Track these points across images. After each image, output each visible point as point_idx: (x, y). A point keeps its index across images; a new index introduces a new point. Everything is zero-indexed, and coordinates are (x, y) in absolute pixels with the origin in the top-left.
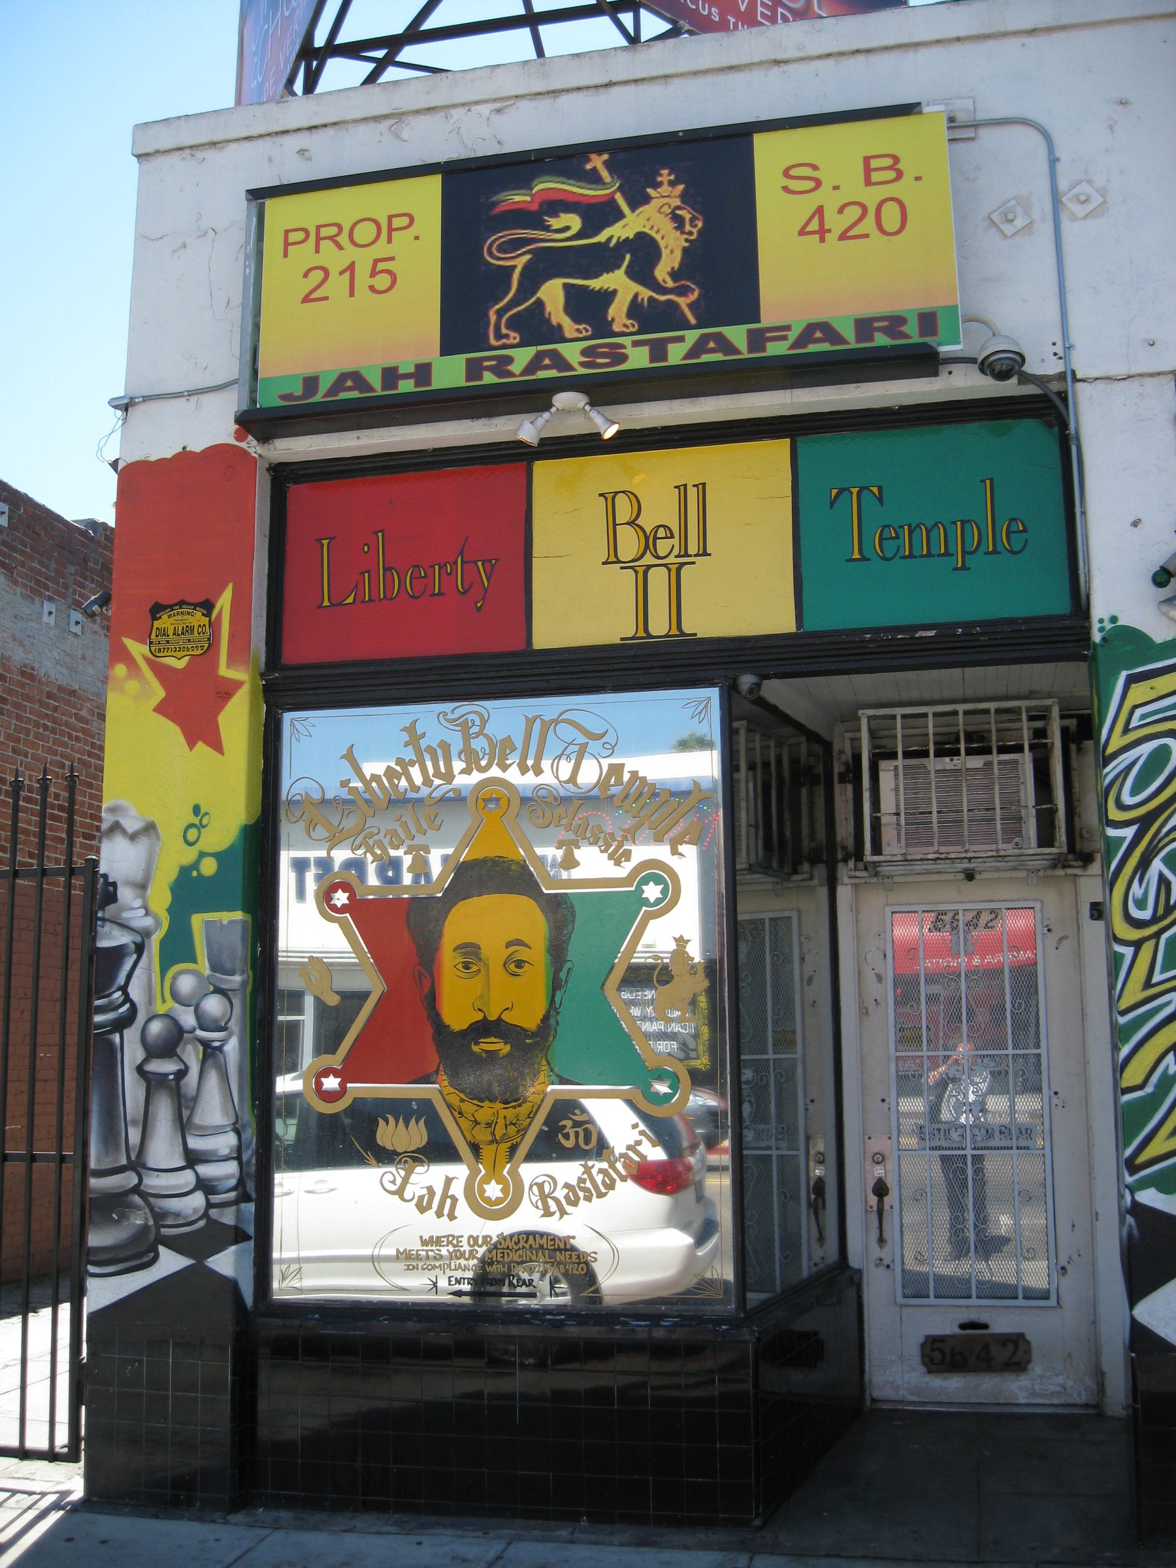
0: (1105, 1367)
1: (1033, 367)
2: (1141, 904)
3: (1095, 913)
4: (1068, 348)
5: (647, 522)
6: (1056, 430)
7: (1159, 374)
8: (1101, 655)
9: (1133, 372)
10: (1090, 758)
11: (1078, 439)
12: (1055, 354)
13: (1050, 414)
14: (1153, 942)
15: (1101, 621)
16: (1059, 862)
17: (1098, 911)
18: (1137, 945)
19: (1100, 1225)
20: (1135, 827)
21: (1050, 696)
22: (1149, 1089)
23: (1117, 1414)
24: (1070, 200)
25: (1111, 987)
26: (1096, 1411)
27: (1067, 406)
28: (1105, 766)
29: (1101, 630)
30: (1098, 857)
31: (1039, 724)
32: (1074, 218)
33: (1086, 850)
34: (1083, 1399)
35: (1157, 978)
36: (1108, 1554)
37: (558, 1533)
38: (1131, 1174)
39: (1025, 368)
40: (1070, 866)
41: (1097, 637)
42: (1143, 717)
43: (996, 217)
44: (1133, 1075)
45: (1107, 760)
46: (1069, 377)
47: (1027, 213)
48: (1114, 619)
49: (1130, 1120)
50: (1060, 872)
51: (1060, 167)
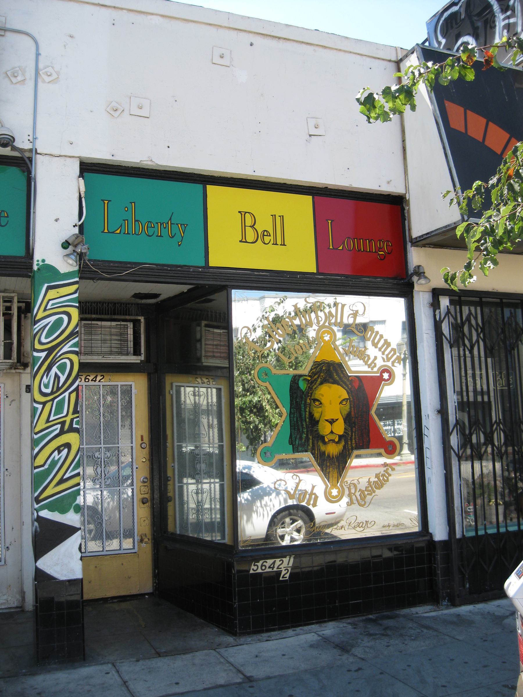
0: (25, 590)
1: (18, 144)
2: (46, 386)
3: (28, 389)
4: (35, 139)
5: (260, 228)
6: (26, 173)
7: (73, 157)
8: (37, 276)
9: (62, 154)
10: (29, 321)
11: (35, 179)
12: (29, 140)
13: (24, 166)
14: (51, 402)
15: (38, 261)
16: (13, 367)
17: (29, 389)
18: (44, 404)
19: (25, 527)
20: (46, 352)
21: (14, 292)
22: (46, 466)
23: (30, 610)
24: (43, 73)
25: (32, 422)
26: (21, 609)
27: (31, 164)
28: (35, 325)
29: (38, 265)
30: (30, 365)
31: (8, 304)
32: (44, 81)
33: (25, 362)
34: (15, 605)
35: (52, 418)
36: (24, 671)
37: (414, 610)
38: (37, 504)
39: (15, 144)
40: (18, 369)
41: (35, 268)
42: (53, 305)
43: (9, 73)
44: (39, 461)
45: (36, 323)
46: (34, 151)
47: (23, 74)
48: (43, 261)
49: (37, 480)
50: (13, 371)
51: (40, 58)
